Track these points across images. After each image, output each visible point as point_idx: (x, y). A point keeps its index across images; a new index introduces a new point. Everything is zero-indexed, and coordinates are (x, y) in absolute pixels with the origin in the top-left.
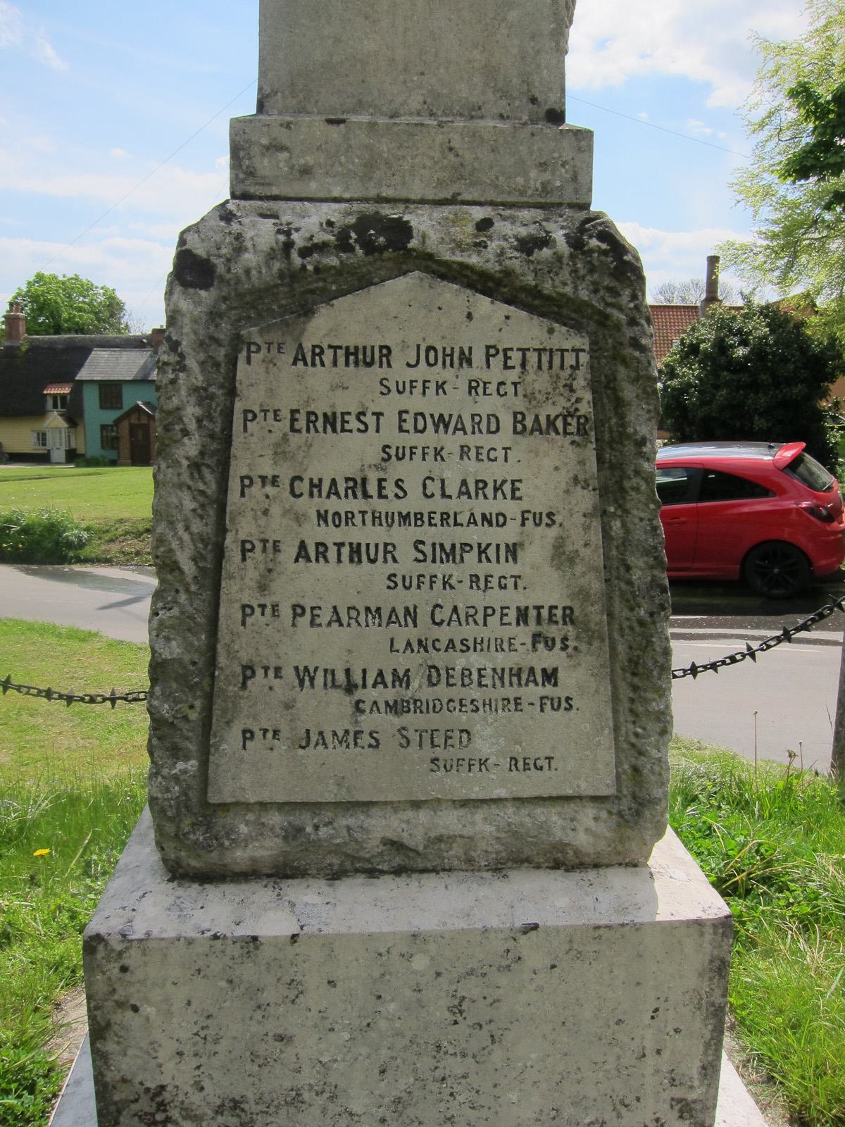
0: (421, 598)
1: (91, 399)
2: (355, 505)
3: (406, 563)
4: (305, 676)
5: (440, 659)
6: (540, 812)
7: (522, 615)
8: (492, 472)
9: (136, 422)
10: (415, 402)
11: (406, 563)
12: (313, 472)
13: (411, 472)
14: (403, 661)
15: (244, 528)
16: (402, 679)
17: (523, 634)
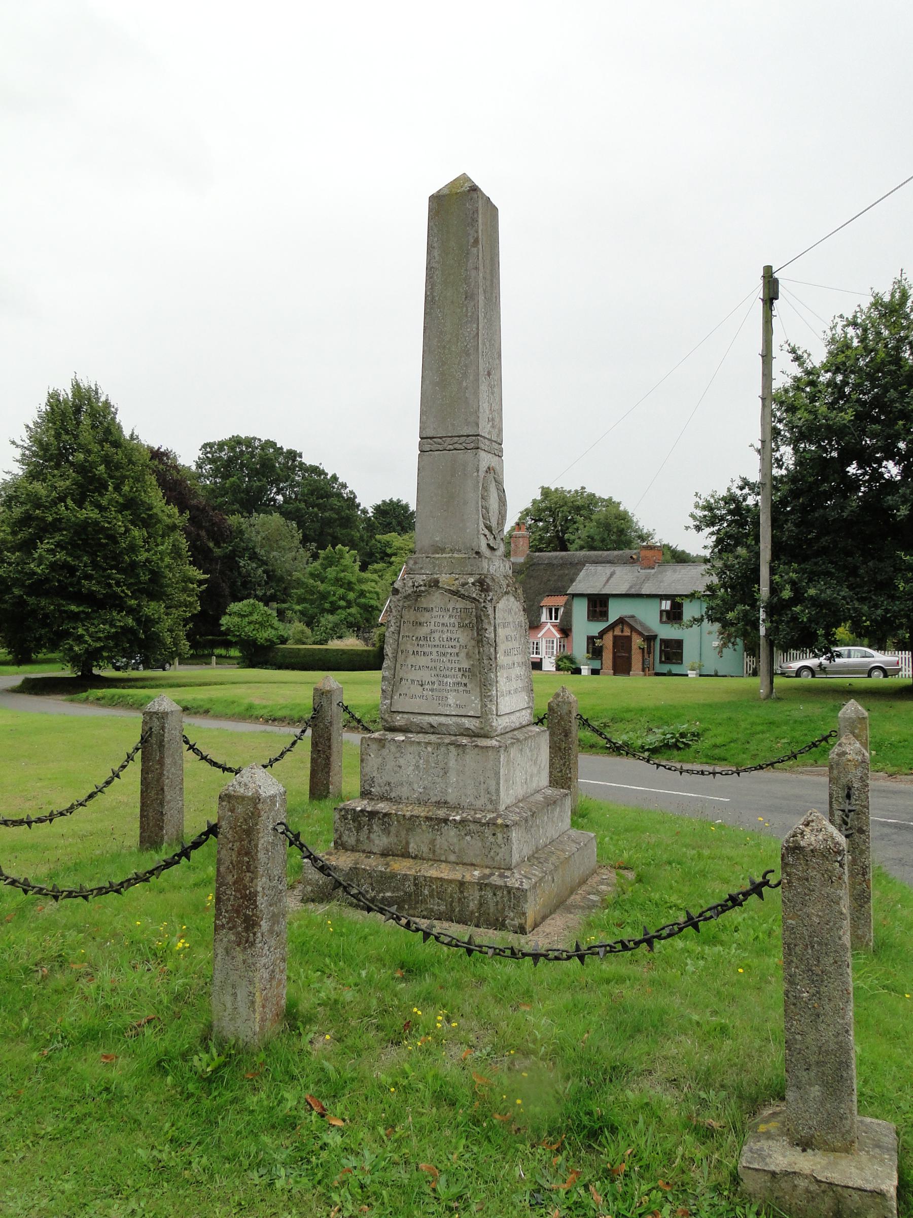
0: (438, 665)
1: (580, 609)
2: (424, 643)
3: (435, 656)
4: (413, 681)
5: (441, 679)
6: (463, 719)
7: (460, 669)
8: (454, 636)
9: (620, 634)
10: (438, 620)
11: (435, 656)
12: (417, 635)
13: (437, 635)
14: (433, 679)
15: (402, 647)
16: (433, 683)
17: (460, 674)
